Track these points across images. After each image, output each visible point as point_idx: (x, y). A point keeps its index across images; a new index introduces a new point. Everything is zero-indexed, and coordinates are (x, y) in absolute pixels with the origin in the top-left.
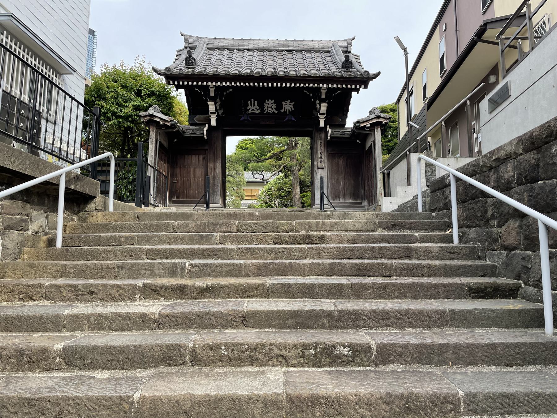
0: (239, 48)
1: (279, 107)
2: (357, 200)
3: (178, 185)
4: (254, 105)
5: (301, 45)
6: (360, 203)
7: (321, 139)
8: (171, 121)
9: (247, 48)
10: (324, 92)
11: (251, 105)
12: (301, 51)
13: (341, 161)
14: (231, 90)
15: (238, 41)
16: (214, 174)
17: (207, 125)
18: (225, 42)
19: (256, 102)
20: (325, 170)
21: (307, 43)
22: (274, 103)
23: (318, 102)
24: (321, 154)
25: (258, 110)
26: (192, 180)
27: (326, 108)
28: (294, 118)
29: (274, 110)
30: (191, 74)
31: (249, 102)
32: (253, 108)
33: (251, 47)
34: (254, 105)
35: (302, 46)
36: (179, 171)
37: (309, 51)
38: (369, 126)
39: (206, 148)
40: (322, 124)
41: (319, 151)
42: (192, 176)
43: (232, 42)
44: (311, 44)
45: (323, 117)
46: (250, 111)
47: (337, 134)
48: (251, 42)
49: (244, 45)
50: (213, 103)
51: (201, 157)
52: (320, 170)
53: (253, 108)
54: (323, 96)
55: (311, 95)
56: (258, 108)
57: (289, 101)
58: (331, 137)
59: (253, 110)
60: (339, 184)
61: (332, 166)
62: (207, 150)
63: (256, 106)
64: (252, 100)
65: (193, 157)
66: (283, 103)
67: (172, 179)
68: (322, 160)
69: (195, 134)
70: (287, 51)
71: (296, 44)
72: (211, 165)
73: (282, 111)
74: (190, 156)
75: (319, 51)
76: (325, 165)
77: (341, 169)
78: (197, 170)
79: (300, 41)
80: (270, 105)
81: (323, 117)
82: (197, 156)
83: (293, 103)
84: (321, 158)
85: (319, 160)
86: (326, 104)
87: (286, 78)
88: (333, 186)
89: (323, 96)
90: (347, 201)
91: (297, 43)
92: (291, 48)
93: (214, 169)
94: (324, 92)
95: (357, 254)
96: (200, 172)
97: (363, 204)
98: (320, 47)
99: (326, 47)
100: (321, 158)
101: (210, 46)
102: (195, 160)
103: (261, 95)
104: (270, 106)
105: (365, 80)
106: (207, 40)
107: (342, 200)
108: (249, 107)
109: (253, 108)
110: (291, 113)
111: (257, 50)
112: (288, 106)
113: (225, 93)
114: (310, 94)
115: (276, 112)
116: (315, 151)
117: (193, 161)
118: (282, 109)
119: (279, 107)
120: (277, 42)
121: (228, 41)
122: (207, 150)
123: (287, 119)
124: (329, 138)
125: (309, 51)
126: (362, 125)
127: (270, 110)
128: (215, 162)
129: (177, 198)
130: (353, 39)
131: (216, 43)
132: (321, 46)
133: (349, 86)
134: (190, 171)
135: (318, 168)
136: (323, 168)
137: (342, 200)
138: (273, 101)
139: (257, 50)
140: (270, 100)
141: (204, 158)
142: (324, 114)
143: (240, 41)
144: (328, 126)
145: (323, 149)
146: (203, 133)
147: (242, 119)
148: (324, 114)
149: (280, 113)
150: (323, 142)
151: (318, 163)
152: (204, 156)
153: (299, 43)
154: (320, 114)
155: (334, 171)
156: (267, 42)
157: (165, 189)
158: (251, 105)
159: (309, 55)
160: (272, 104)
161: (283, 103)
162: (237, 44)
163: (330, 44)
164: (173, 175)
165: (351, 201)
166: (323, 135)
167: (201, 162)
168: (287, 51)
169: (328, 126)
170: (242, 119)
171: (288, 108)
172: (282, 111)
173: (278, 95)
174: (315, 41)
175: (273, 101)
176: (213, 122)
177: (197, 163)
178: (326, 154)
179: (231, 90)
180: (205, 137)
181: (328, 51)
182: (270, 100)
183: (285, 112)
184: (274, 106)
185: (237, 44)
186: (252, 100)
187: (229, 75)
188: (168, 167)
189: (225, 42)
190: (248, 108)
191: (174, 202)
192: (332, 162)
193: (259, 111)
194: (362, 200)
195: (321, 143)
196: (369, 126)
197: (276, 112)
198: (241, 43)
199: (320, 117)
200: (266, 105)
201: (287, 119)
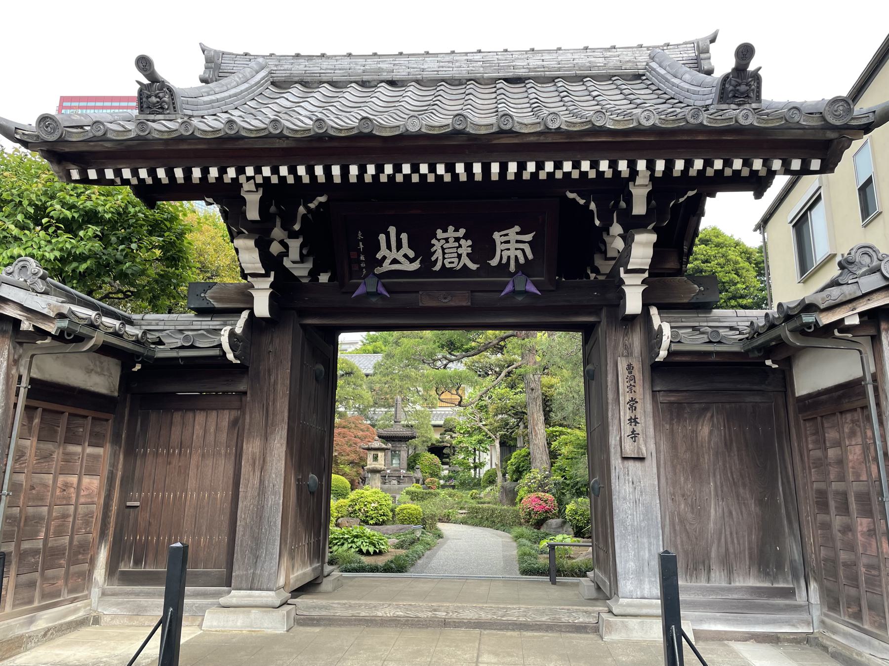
0: (365, 78)
1: (483, 249)
2: (775, 579)
3: (144, 517)
4: (399, 246)
5: (551, 62)
6: (789, 593)
7: (629, 354)
8: (61, 316)
9: (389, 77)
10: (640, 193)
11: (389, 247)
12: (552, 80)
13: (705, 430)
14: (323, 199)
15: (361, 61)
16: (261, 482)
17: (245, 315)
18: (325, 64)
19: (404, 237)
20: (651, 464)
21: (569, 56)
22: (466, 237)
23: (616, 229)
24: (633, 408)
25: (412, 261)
26: (192, 496)
27: (650, 252)
28: (535, 284)
29: (466, 260)
30: (138, 138)
31: (382, 237)
32: (395, 254)
33: (397, 75)
34: (399, 246)
35: (554, 64)
36: (151, 467)
37: (579, 79)
38: (856, 321)
39: (242, 387)
40: (633, 304)
41: (624, 398)
42: (192, 483)
43: (346, 63)
44: (582, 60)
45: (638, 279)
46: (387, 266)
47: (694, 343)
48: (402, 60)
49: (380, 70)
50: (251, 243)
51: (226, 417)
52: (631, 464)
53: (394, 254)
54: (639, 208)
55: (593, 206)
56: (411, 254)
57: (517, 228)
58: (670, 353)
59: (395, 261)
60: (700, 511)
61: (674, 447)
62: (245, 393)
63: (406, 249)
64: (392, 230)
65: (200, 417)
66: (496, 236)
67: (124, 497)
68: (636, 422)
69: (192, 347)
70: (507, 80)
71: (535, 62)
72: (252, 447)
73: (494, 262)
74: (190, 415)
75: (609, 77)
76: (648, 446)
77: (707, 460)
78: (209, 462)
79: (549, 51)
80: (452, 243)
81: (638, 279)
82: (214, 414)
83: (529, 237)
84: (633, 421)
85: (627, 429)
86: (653, 237)
87: (502, 143)
88: (682, 522)
89: (639, 208)
90: (740, 582)
91: (539, 57)
92: (521, 72)
93: (262, 463)
94: (640, 193)
95: (457, 82)
96: (223, 468)
97: (800, 598)
98: (611, 64)
99: (629, 66)
100: (633, 421)
101: (280, 75)
102: (206, 427)
103: (421, 210)
104: (452, 248)
105: (831, 135)
106: (272, 62)
107: (718, 579)
108: (383, 251)
109: (395, 254)
110: (525, 269)
111: (417, 81)
112: (512, 245)
113: (302, 210)
114: (587, 205)
115: (473, 266)
116: (611, 396)
117: (198, 431)
118: (493, 256)
119: (483, 249)
120: (478, 57)
121: (333, 62)
122: (245, 393)
123: (509, 288)
124: (663, 354)
125: (579, 79)
126: (826, 319)
127: (452, 262)
128: (266, 438)
129: (137, 563)
130: (713, 40)
131: (299, 69)
132: (613, 62)
133: (757, 164)
134: (187, 467)
135: (625, 459)
136: (642, 459)
137: (718, 579)
138: (462, 231)
139: (417, 81)
140: (451, 228)
141: (234, 423)
142: (642, 271)
143: (369, 61)
144: (654, 311)
145: (639, 389)
146: (220, 346)
147: (360, 291)
148: (642, 271)
149: (485, 269)
150: (637, 365)
151: (619, 437)
152: (235, 413)
153: (546, 57)
154: (628, 271)
155: (682, 464)
156: (447, 58)
157: (94, 535)
158: (389, 247)
159: (577, 88)
160: (457, 240)
161: (496, 236)
162: (359, 69)
163: (643, 58)
164: (128, 482)
165: (752, 582)
166: (636, 340)
167: (223, 437)
168: (507, 80)
169: (654, 311)
170: (360, 291)
171: (512, 253)
172: (494, 262)
173: (481, 209)
174: (594, 50)
175: (462, 231)
176: (262, 307)
177: (211, 438)
178: (649, 407)
179: (323, 199)
180: (230, 356)
181: (638, 77)
182: (451, 228)
183: (503, 267)
184: (466, 246)
185: (358, 67)
186: (392, 230)
187: (281, 136)
188: (115, 455)
189: (325, 64)
190: (379, 256)
191: (128, 579)
192: (672, 431)
193: (416, 266)
194: (796, 577)
195: (630, 368)
196: (856, 321)
197: (473, 266)
198: (371, 64)
199: (627, 279)
200: (437, 245)
201: (509, 288)
